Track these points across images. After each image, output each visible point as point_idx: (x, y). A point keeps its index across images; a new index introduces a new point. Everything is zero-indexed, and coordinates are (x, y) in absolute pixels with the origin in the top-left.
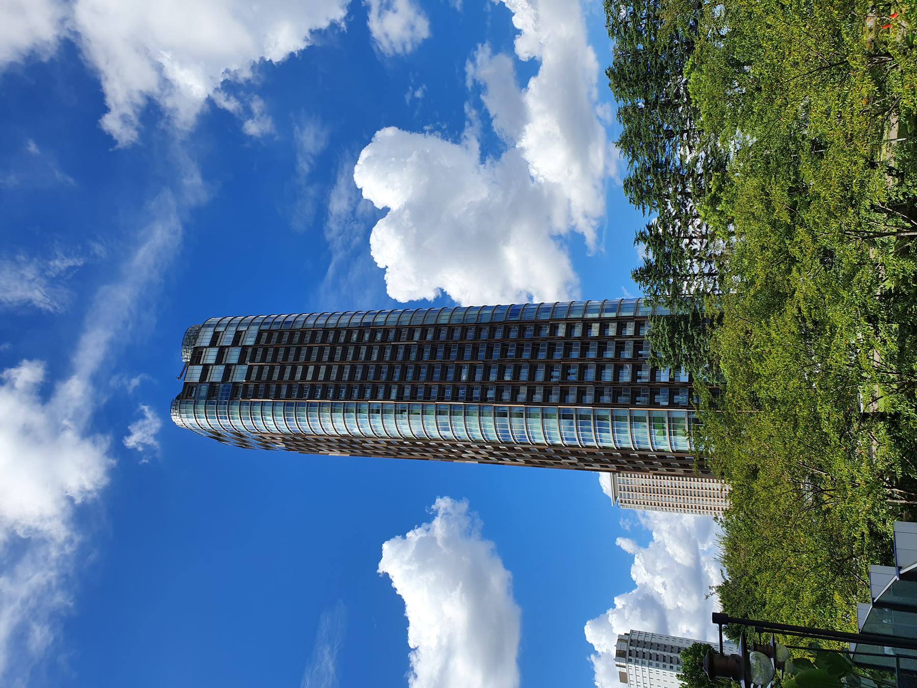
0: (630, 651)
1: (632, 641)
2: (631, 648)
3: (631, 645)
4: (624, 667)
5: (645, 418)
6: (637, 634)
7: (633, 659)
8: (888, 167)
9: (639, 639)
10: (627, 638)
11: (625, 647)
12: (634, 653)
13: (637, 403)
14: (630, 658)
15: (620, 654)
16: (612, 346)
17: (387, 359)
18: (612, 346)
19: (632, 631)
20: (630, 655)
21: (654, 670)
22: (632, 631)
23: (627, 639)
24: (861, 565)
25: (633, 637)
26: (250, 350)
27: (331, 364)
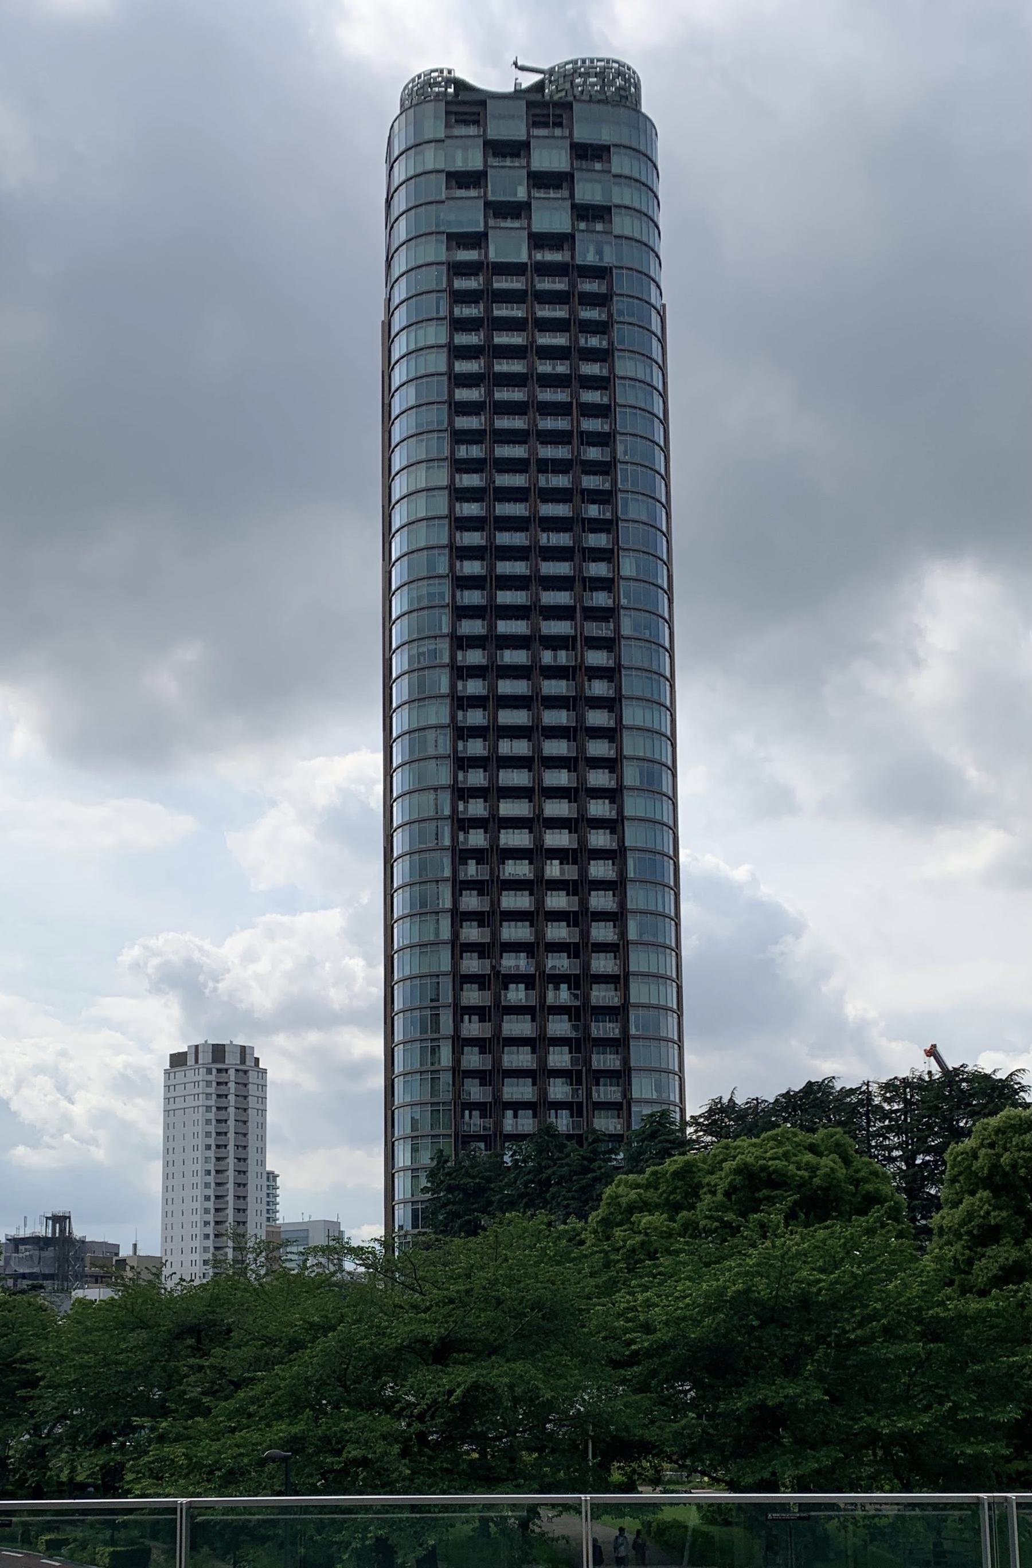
0: (226, 1070)
1: (246, 1072)
2: (232, 1072)
3: (237, 1070)
4: (197, 1062)
5: (451, 1135)
6: (260, 1082)
7: (212, 1077)
8: (920, 1322)
9: (250, 1086)
10: (250, 1062)
11: (232, 1060)
12: (223, 1077)
13: (467, 1112)
14: (214, 1071)
15: (218, 1052)
16: (571, 872)
17: (497, 368)
18: (571, 872)
19: (265, 1071)
20: (219, 1071)
21: (200, 1115)
22: (265, 1071)
23: (248, 1063)
24: (559, 1362)
25: (252, 1076)
26: (457, 117)
27: (578, 615)
